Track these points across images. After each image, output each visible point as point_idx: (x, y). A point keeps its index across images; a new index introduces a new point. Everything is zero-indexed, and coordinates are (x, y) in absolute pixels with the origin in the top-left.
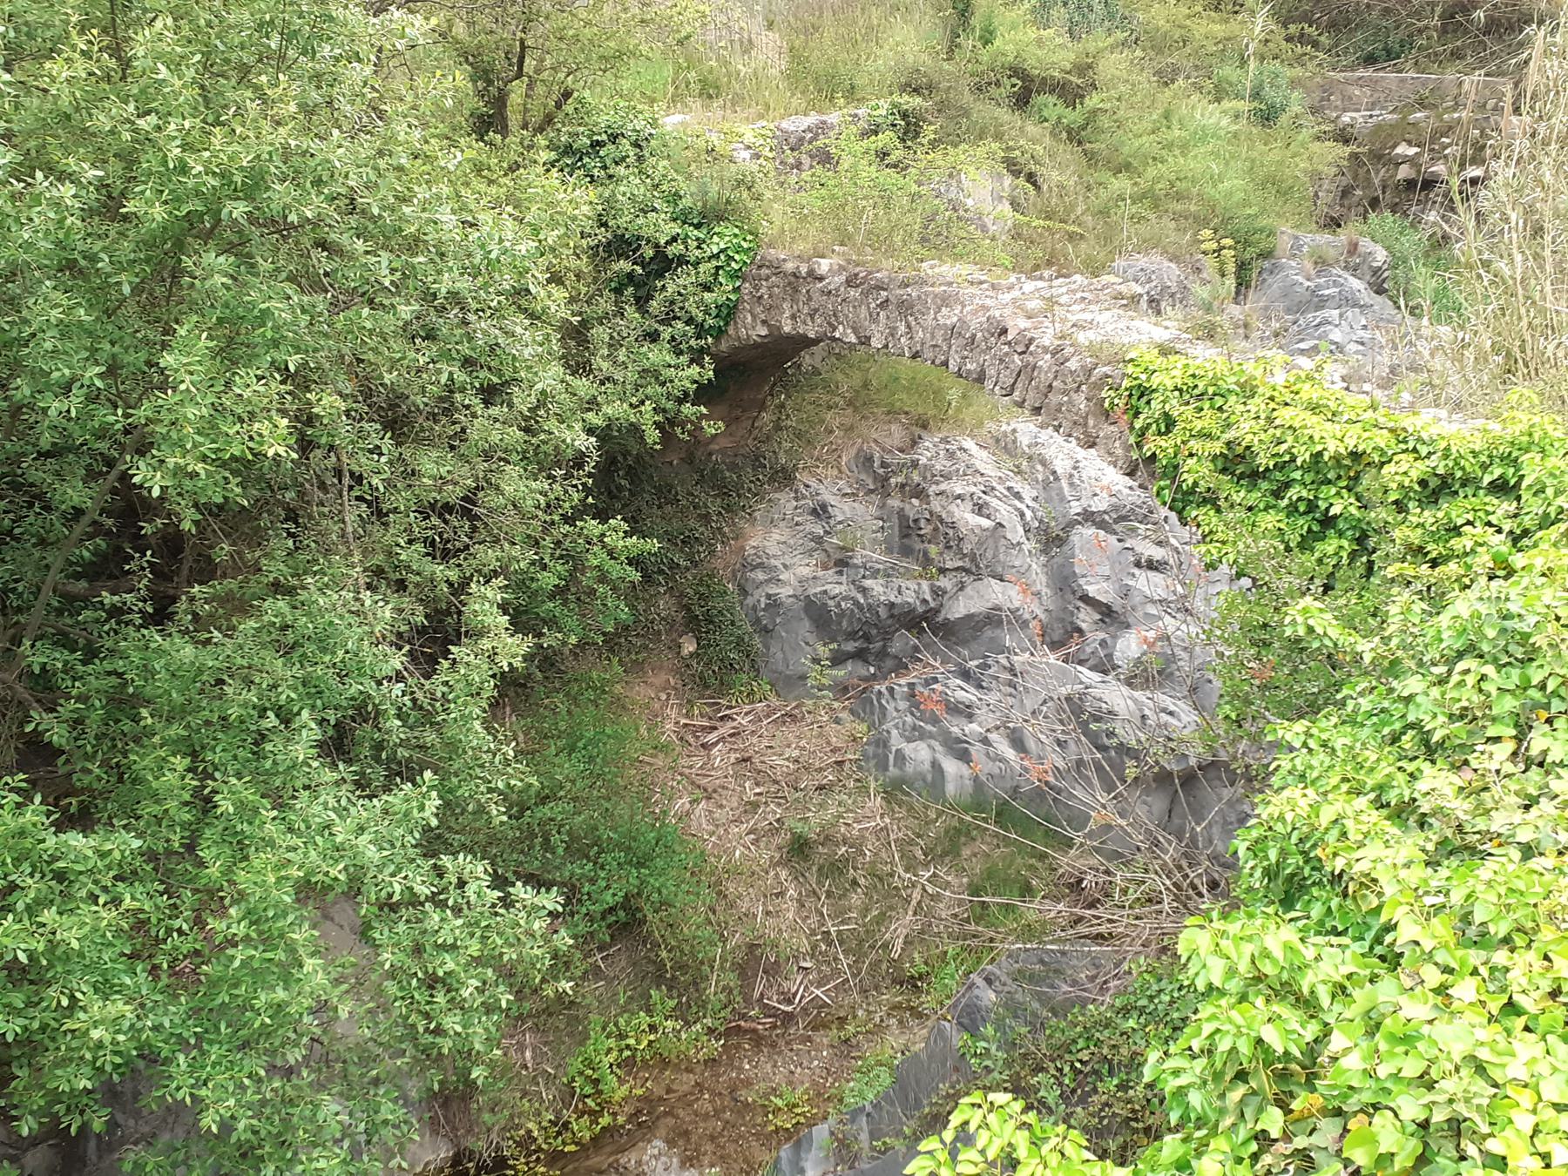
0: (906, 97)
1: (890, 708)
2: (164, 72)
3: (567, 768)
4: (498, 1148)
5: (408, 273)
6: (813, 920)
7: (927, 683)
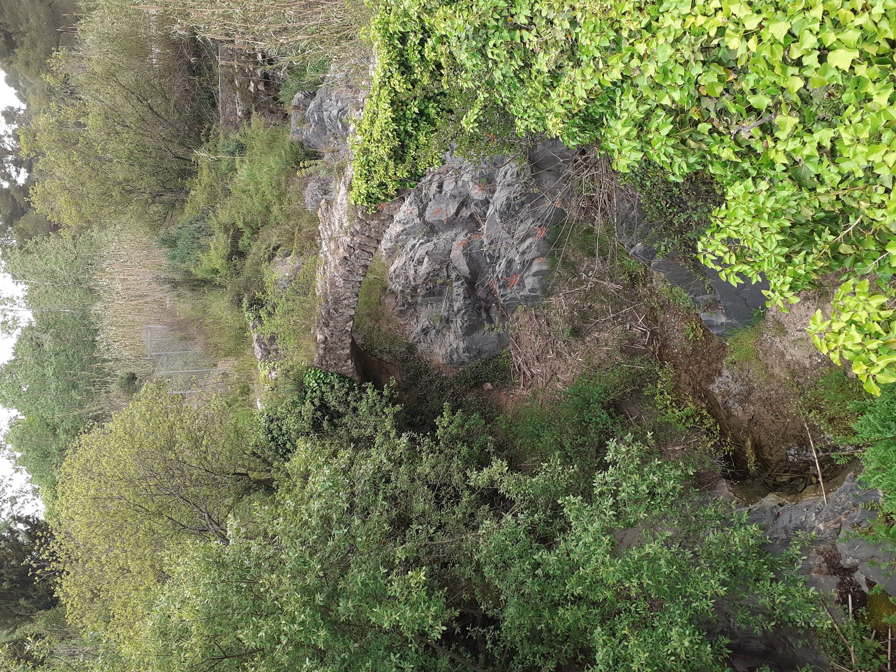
0: (244, 305)
1: (510, 296)
2: (262, 634)
3: (548, 438)
4: (720, 459)
5: (339, 521)
6: (608, 325)
7: (498, 280)
